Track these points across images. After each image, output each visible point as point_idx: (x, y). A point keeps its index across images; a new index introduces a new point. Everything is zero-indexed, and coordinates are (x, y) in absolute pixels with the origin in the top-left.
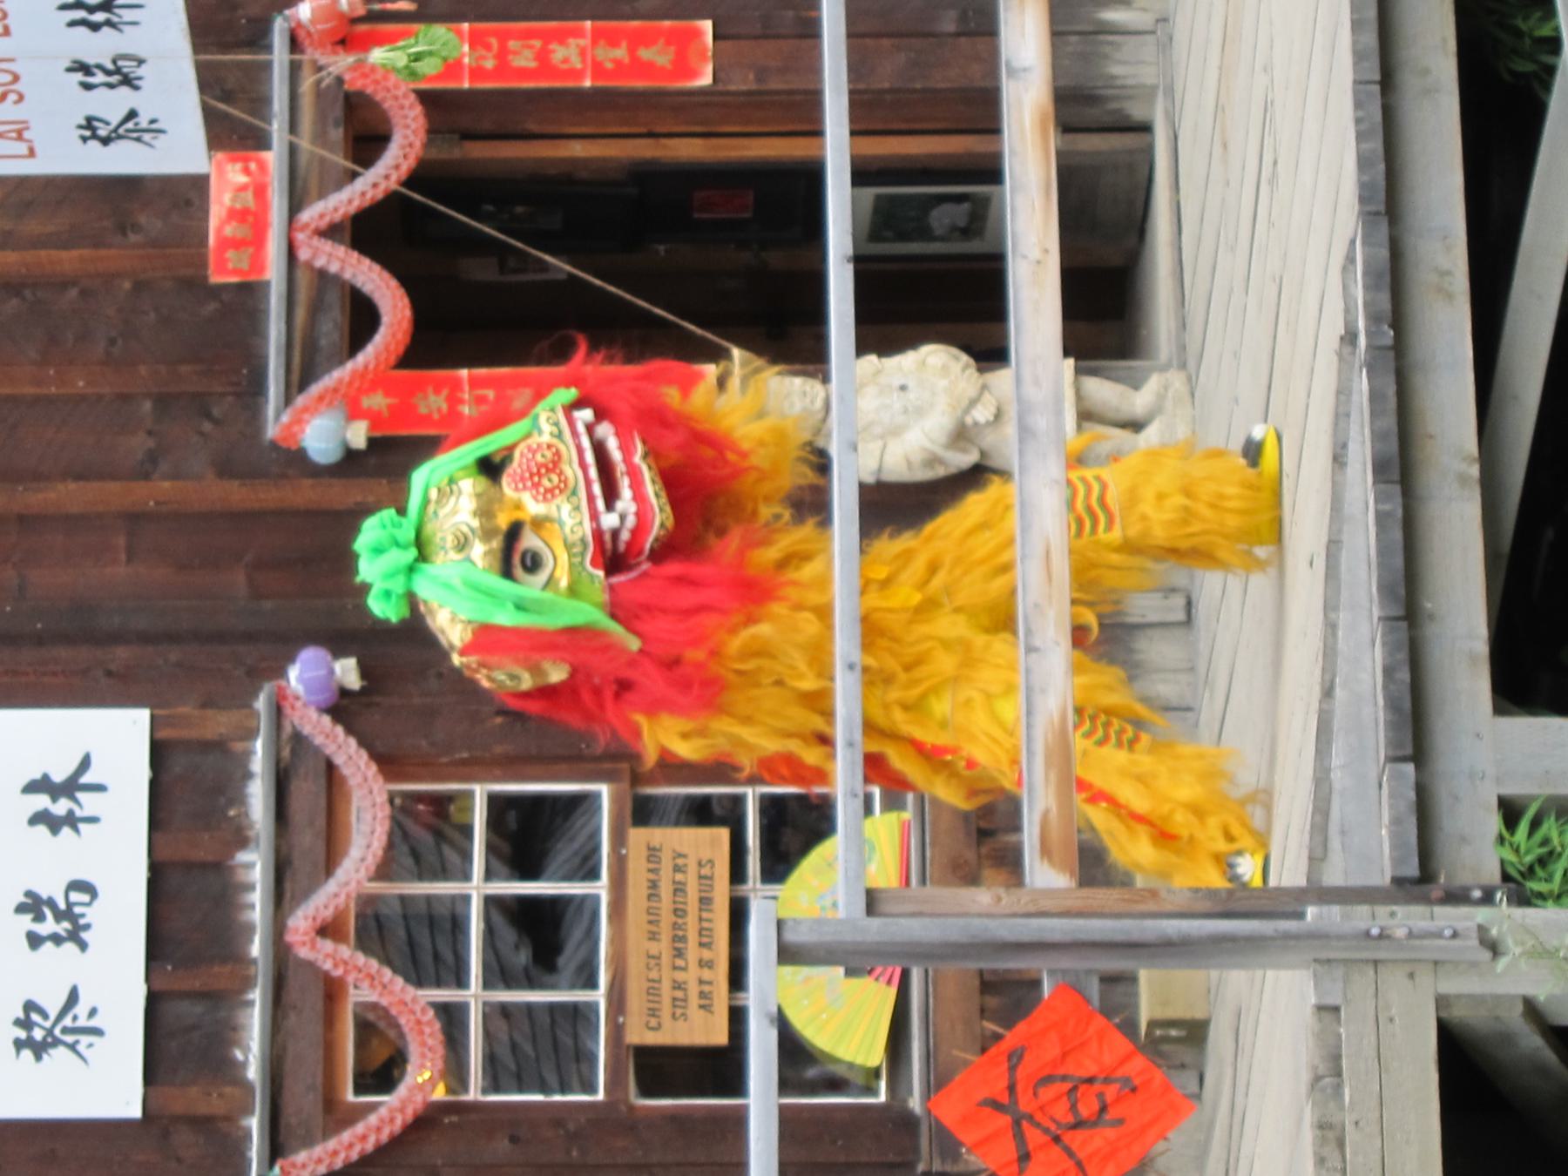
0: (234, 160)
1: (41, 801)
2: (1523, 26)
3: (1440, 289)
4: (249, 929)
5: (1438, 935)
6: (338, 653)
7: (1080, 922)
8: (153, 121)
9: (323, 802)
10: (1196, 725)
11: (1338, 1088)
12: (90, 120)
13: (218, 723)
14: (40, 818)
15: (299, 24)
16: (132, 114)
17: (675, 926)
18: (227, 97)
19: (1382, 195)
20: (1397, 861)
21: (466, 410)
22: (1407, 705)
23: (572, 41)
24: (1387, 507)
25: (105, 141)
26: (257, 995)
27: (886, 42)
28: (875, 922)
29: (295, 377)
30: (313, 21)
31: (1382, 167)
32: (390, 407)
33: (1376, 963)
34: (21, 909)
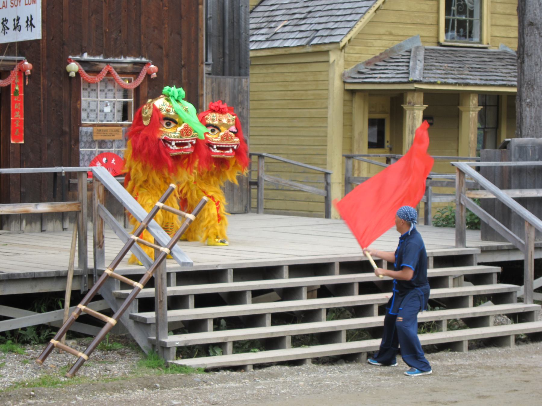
2: (43, 305)
8: (7, 33)
15: (24, 62)
16: (8, 29)
18: (9, 47)
19: (12, 278)
23: (20, 116)
25: (2, 23)
30: (25, 65)
31: (18, 278)
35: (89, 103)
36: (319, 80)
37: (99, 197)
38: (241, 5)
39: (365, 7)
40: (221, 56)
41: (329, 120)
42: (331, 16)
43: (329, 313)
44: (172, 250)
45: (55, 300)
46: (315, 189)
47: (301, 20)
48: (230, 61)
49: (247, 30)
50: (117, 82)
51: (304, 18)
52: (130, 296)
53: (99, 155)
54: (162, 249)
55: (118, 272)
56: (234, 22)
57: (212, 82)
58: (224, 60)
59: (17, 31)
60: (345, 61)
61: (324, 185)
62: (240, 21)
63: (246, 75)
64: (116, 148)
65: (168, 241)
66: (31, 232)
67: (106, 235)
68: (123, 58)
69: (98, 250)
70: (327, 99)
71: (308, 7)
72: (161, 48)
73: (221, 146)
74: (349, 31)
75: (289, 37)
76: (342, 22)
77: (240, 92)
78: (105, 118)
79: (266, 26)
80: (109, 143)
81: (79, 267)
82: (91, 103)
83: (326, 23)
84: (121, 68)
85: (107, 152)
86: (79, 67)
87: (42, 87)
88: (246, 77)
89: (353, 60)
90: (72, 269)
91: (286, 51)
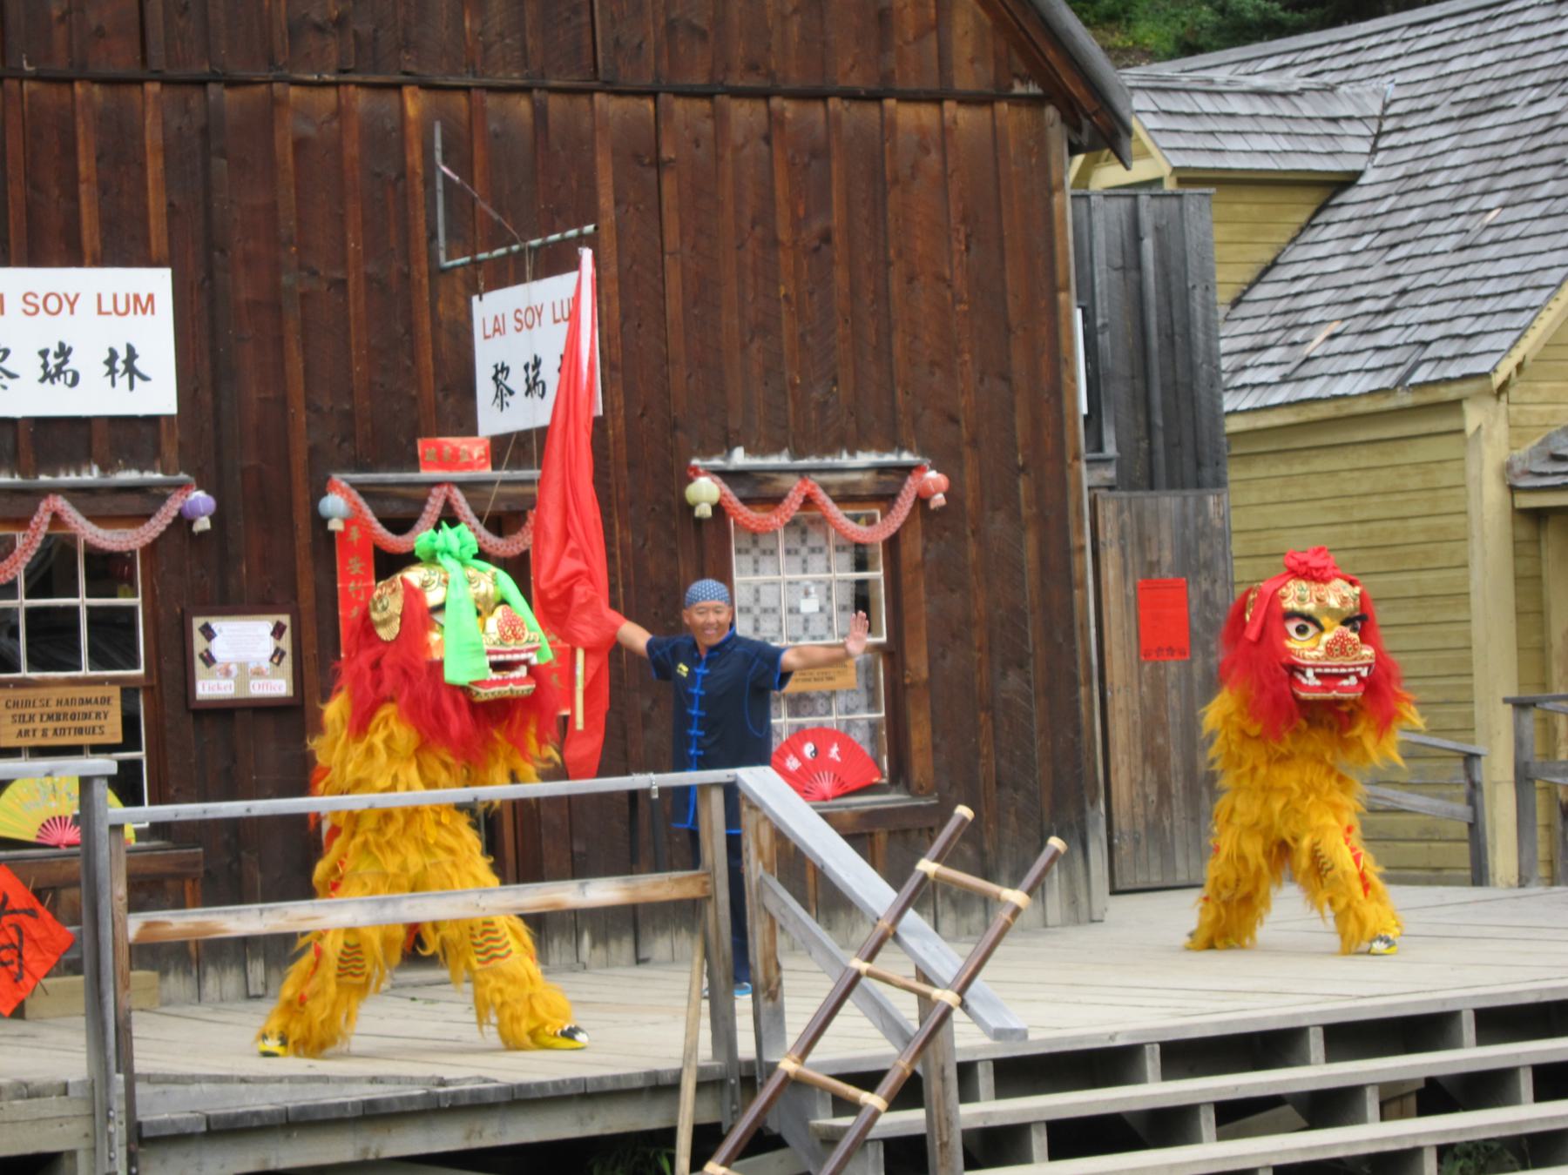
0: (486, 450)
1: (123, 354)
3: (472, 1131)
4: (54, 474)
5: (111, 1150)
6: (212, 519)
7: (111, 946)
9: (129, 513)
10: (191, 1004)
11: (21, 1097)
12: (507, 369)
13: (170, 451)
14: (113, 355)
16: (511, 393)
17: (65, 715)
20: (151, 1124)
21: (352, 585)
22: (239, 1125)
24: (349, 1108)
25: (495, 378)
26: (17, 479)
27: (566, 812)
28: (106, 830)
29: (366, 489)
32: (352, 543)
33: (93, 1115)
34: (62, 345)
35: (757, 591)
36: (1437, 485)
37: (760, 853)
38: (1190, 285)
39: (1560, 266)
40: (1142, 433)
41: (1475, 600)
42: (1464, 299)
43: (1446, 1160)
44: (968, 995)
45: (651, 1155)
46: (1437, 803)
47: (1379, 317)
48: (1168, 446)
49: (1213, 357)
50: (834, 525)
51: (1387, 311)
52: (850, 1131)
53: (792, 736)
54: (936, 993)
55: (817, 1067)
56: (1173, 334)
57: (1120, 511)
58: (1150, 444)
59: (536, 397)
60: (1510, 426)
61: (1464, 790)
62: (1192, 330)
63: (1219, 483)
64: (840, 714)
65: (955, 971)
66: (608, 965)
67: (786, 962)
68: (845, 456)
69: (766, 1005)
70: (1465, 540)
71: (1397, 277)
72: (954, 420)
73: (1327, 670)
74: (1517, 340)
75: (1347, 368)
76: (1494, 313)
77: (1201, 534)
78: (806, 629)
79: (1279, 340)
80: (821, 701)
81: (715, 1056)
82: (763, 589)
83: (1450, 320)
84: (844, 486)
85: (815, 726)
86: (721, 489)
87: (618, 552)
88: (1219, 490)
89: (1535, 421)
90: (693, 1064)
91: (1338, 408)
